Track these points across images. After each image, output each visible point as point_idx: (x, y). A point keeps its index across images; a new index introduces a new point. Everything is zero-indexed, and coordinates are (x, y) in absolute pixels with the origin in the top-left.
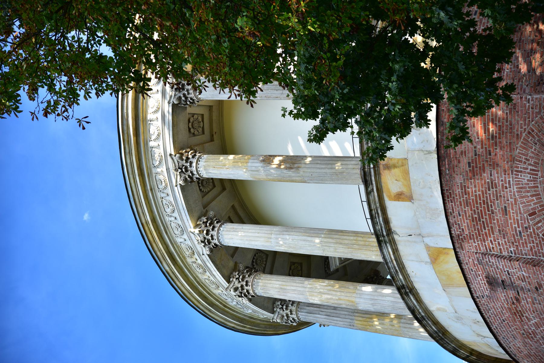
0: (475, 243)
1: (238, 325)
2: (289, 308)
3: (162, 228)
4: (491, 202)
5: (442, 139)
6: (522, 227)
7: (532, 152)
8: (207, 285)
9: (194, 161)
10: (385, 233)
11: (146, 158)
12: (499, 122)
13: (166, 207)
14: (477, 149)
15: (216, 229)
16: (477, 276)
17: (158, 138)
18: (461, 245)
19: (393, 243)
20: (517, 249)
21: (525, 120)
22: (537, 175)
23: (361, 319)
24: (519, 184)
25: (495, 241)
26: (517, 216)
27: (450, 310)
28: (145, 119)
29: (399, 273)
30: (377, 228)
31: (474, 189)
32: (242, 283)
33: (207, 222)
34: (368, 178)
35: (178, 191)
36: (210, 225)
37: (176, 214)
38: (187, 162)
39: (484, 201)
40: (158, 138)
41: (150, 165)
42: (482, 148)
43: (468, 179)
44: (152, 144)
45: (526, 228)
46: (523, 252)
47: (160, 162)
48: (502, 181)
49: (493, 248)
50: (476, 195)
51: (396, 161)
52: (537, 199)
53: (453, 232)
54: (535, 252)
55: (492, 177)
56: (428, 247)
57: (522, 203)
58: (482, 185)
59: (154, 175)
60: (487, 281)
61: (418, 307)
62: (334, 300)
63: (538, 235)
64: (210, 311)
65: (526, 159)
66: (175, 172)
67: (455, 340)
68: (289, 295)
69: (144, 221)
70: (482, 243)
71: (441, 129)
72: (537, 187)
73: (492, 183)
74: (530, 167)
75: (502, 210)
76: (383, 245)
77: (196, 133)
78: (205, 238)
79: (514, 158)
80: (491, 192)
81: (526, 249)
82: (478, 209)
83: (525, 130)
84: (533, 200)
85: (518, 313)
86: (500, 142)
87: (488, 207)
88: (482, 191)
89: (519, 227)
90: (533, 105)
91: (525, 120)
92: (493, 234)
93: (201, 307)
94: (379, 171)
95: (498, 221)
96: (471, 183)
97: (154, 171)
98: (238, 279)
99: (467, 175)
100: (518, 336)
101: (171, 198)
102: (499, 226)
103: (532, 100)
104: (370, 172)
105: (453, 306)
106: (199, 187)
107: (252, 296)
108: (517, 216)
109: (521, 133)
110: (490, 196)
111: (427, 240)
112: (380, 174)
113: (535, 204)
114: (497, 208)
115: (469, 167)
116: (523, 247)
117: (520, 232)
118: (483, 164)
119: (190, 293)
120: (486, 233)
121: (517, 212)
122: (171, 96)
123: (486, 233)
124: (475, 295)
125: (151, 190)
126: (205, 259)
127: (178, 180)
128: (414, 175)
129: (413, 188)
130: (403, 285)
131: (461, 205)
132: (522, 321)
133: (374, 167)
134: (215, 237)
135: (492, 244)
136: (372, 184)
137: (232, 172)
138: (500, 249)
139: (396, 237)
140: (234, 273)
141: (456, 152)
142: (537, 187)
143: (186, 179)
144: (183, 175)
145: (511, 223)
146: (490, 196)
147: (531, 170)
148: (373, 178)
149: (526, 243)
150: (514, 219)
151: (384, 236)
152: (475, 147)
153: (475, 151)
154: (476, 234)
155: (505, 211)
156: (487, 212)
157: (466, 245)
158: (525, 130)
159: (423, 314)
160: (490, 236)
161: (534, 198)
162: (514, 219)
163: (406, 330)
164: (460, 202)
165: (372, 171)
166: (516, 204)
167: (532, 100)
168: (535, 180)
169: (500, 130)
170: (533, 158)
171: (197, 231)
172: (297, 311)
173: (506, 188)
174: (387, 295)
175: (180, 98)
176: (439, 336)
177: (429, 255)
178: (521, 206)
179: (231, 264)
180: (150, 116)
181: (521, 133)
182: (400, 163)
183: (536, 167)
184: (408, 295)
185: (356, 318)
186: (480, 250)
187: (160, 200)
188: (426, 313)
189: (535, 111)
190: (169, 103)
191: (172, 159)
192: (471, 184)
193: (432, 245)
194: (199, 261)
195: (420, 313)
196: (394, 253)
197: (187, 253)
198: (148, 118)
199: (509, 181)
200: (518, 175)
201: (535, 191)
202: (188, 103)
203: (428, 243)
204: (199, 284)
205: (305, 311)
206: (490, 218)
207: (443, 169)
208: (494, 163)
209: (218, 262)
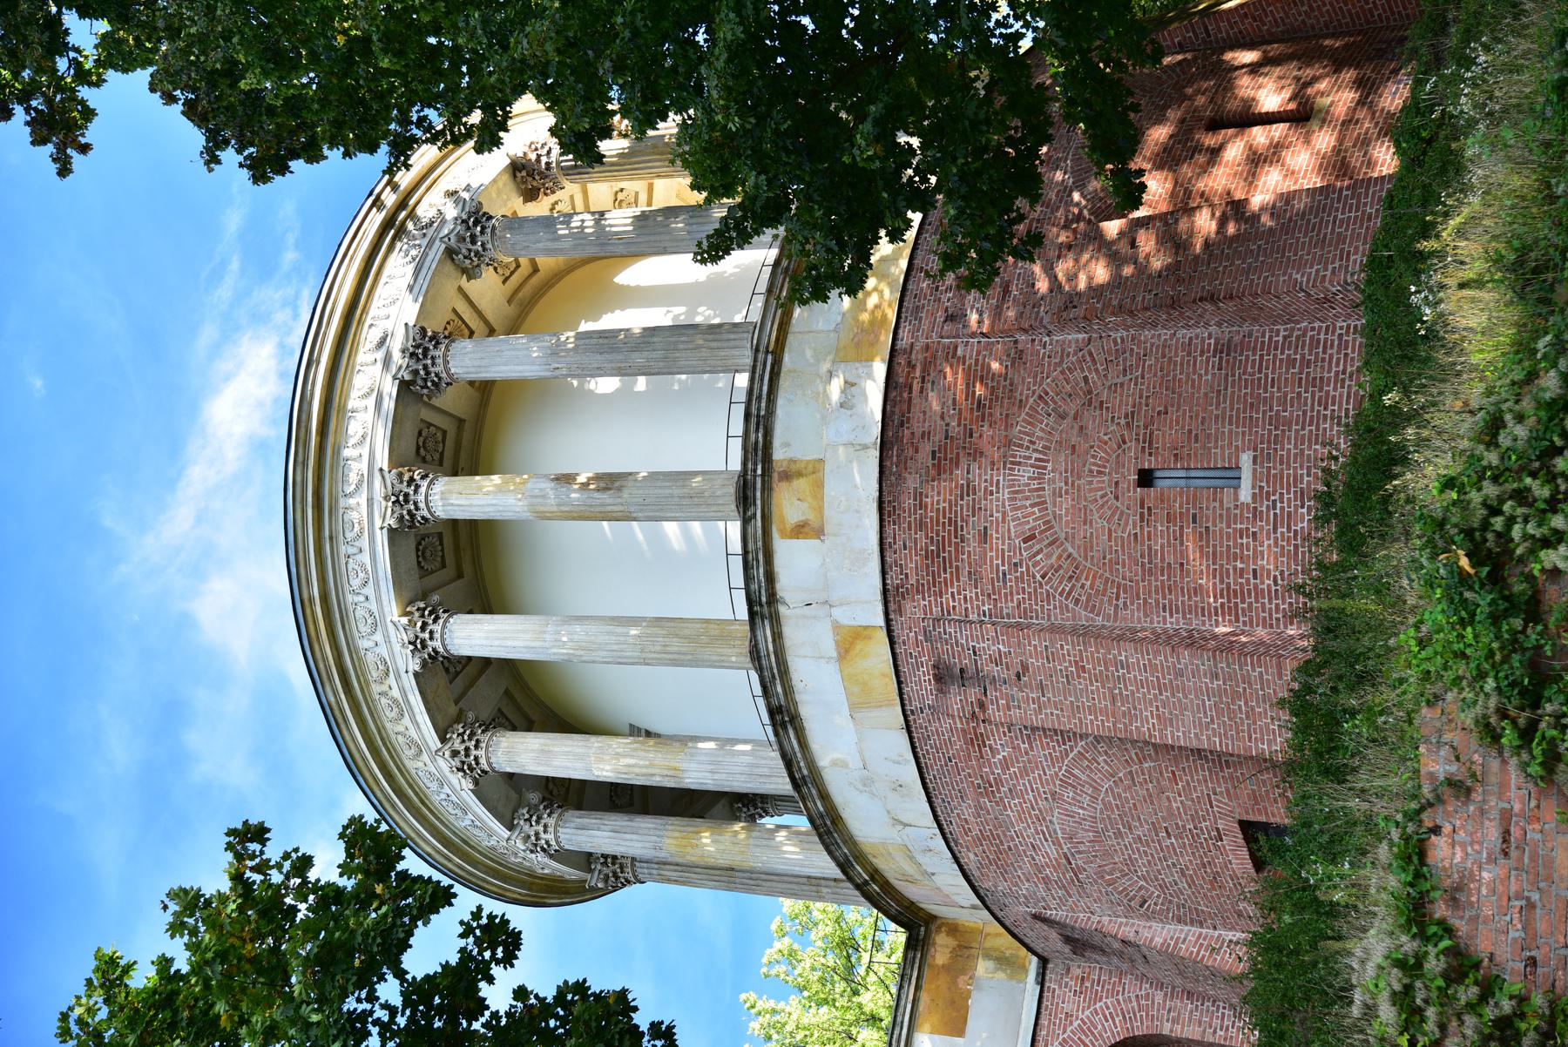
0: (924, 599)
1: (438, 852)
2: (543, 821)
3: (337, 616)
4: (962, 520)
5: (893, 413)
6: (1009, 564)
7: (1042, 430)
8: (399, 749)
9: (424, 484)
10: (764, 599)
11: (331, 478)
12: (993, 380)
13: (352, 574)
14: (950, 429)
15: (441, 621)
16: (919, 665)
17: (361, 443)
18: (900, 606)
19: (776, 620)
20: (995, 606)
21: (1035, 377)
22: (1045, 468)
23: (677, 834)
24: (1013, 486)
25: (959, 593)
26: (1003, 544)
27: (855, 763)
28: (343, 409)
29: (778, 681)
30: (752, 587)
31: (936, 499)
32: (468, 744)
33: (424, 609)
34: (750, 493)
35: (382, 539)
36: (431, 613)
37: (369, 590)
38: (409, 485)
39: (950, 519)
40: (361, 443)
41: (337, 493)
42: (959, 425)
43: (927, 481)
44: (346, 453)
45: (1015, 564)
46: (1005, 611)
47: (358, 487)
48: (986, 481)
49: (954, 607)
50: (938, 510)
51: (803, 465)
52: (1040, 511)
53: (889, 582)
54: (1025, 609)
55: (970, 476)
56: (837, 627)
57: (1013, 520)
58: (951, 491)
59: (341, 511)
60: (934, 675)
61: (799, 755)
62: (641, 767)
63: (1034, 577)
64: (393, 806)
65: (1031, 442)
66: (384, 503)
67: (850, 841)
68: (556, 763)
69: (306, 596)
70: (936, 600)
71: (893, 394)
72: (1044, 489)
73: (968, 486)
74: (1035, 455)
75: (980, 535)
76: (758, 621)
77: (428, 458)
78: (417, 637)
79: (1010, 441)
80: (964, 503)
81: (1010, 604)
82: (938, 535)
83: (1034, 393)
84: (1034, 513)
85: (977, 740)
86: (991, 415)
87: (956, 531)
88: (950, 501)
89: (1003, 565)
90: (1051, 351)
91: (1035, 377)
92: (958, 581)
93: (379, 793)
94: (770, 483)
95: (969, 556)
96: (933, 487)
97: (342, 503)
98: (462, 735)
99: (928, 472)
100: (969, 792)
101: (366, 558)
102: (970, 564)
103: (1051, 344)
104: (755, 483)
105: (861, 753)
106: (418, 556)
107: (483, 771)
108: (1003, 544)
109: (1027, 398)
110: (962, 509)
111: (836, 612)
112: (771, 489)
113: (1035, 520)
114: (971, 534)
115: (933, 459)
116: (1006, 601)
117: (1004, 574)
118: (958, 454)
119: (364, 759)
120: (945, 579)
121: (1003, 536)
122: (401, 367)
123: (945, 579)
124: (908, 708)
125: (331, 538)
126: (407, 686)
127: (385, 517)
128: (832, 489)
129: (827, 512)
130: (781, 706)
131: (910, 529)
132: (982, 757)
133: (763, 475)
134: (437, 635)
135: (954, 601)
136: (755, 504)
137: (494, 502)
138: (966, 609)
139: (782, 609)
140: (455, 726)
141: (913, 433)
142: (1044, 489)
143: (402, 516)
144: (397, 508)
145: (991, 557)
146: (962, 509)
147: (1036, 460)
148: (758, 494)
149: (1011, 594)
150: (997, 550)
151: (761, 605)
152: (947, 425)
153: (947, 431)
154: (928, 581)
155: (984, 536)
156: (954, 540)
157: (908, 606)
158: (1034, 393)
159: (805, 772)
160: (952, 586)
161: (1036, 509)
162: (997, 550)
163: (758, 850)
164: (910, 523)
165: (759, 480)
166: (1004, 522)
167: (1051, 344)
168: (1040, 477)
169: (992, 394)
170: (1042, 438)
171: (405, 620)
172: (556, 825)
173: (992, 494)
174: (744, 753)
175: (416, 372)
176: (826, 825)
177: (837, 642)
178: (1012, 524)
179: (453, 710)
180: (351, 404)
181: (1027, 398)
182: (810, 468)
183: (1045, 454)
184: (785, 729)
185: (670, 834)
186: (931, 613)
187: (343, 561)
188: (810, 772)
189: (1054, 361)
190: (395, 378)
191: (383, 477)
192: (933, 489)
193: (845, 621)
194: (395, 693)
195: (800, 768)
196: (774, 641)
197: (375, 674)
198: (350, 407)
199: (998, 481)
200: (1013, 469)
201: (1039, 496)
202: (429, 384)
203: (839, 619)
204: (385, 744)
205: (572, 825)
206: (957, 550)
207: (888, 464)
208: (975, 451)
209: (430, 698)
